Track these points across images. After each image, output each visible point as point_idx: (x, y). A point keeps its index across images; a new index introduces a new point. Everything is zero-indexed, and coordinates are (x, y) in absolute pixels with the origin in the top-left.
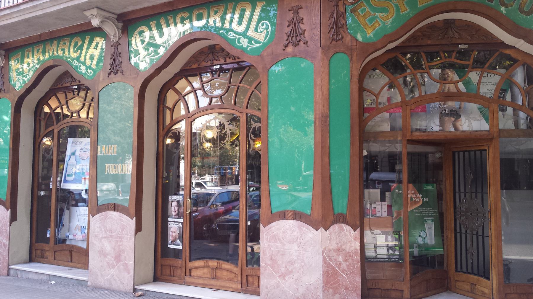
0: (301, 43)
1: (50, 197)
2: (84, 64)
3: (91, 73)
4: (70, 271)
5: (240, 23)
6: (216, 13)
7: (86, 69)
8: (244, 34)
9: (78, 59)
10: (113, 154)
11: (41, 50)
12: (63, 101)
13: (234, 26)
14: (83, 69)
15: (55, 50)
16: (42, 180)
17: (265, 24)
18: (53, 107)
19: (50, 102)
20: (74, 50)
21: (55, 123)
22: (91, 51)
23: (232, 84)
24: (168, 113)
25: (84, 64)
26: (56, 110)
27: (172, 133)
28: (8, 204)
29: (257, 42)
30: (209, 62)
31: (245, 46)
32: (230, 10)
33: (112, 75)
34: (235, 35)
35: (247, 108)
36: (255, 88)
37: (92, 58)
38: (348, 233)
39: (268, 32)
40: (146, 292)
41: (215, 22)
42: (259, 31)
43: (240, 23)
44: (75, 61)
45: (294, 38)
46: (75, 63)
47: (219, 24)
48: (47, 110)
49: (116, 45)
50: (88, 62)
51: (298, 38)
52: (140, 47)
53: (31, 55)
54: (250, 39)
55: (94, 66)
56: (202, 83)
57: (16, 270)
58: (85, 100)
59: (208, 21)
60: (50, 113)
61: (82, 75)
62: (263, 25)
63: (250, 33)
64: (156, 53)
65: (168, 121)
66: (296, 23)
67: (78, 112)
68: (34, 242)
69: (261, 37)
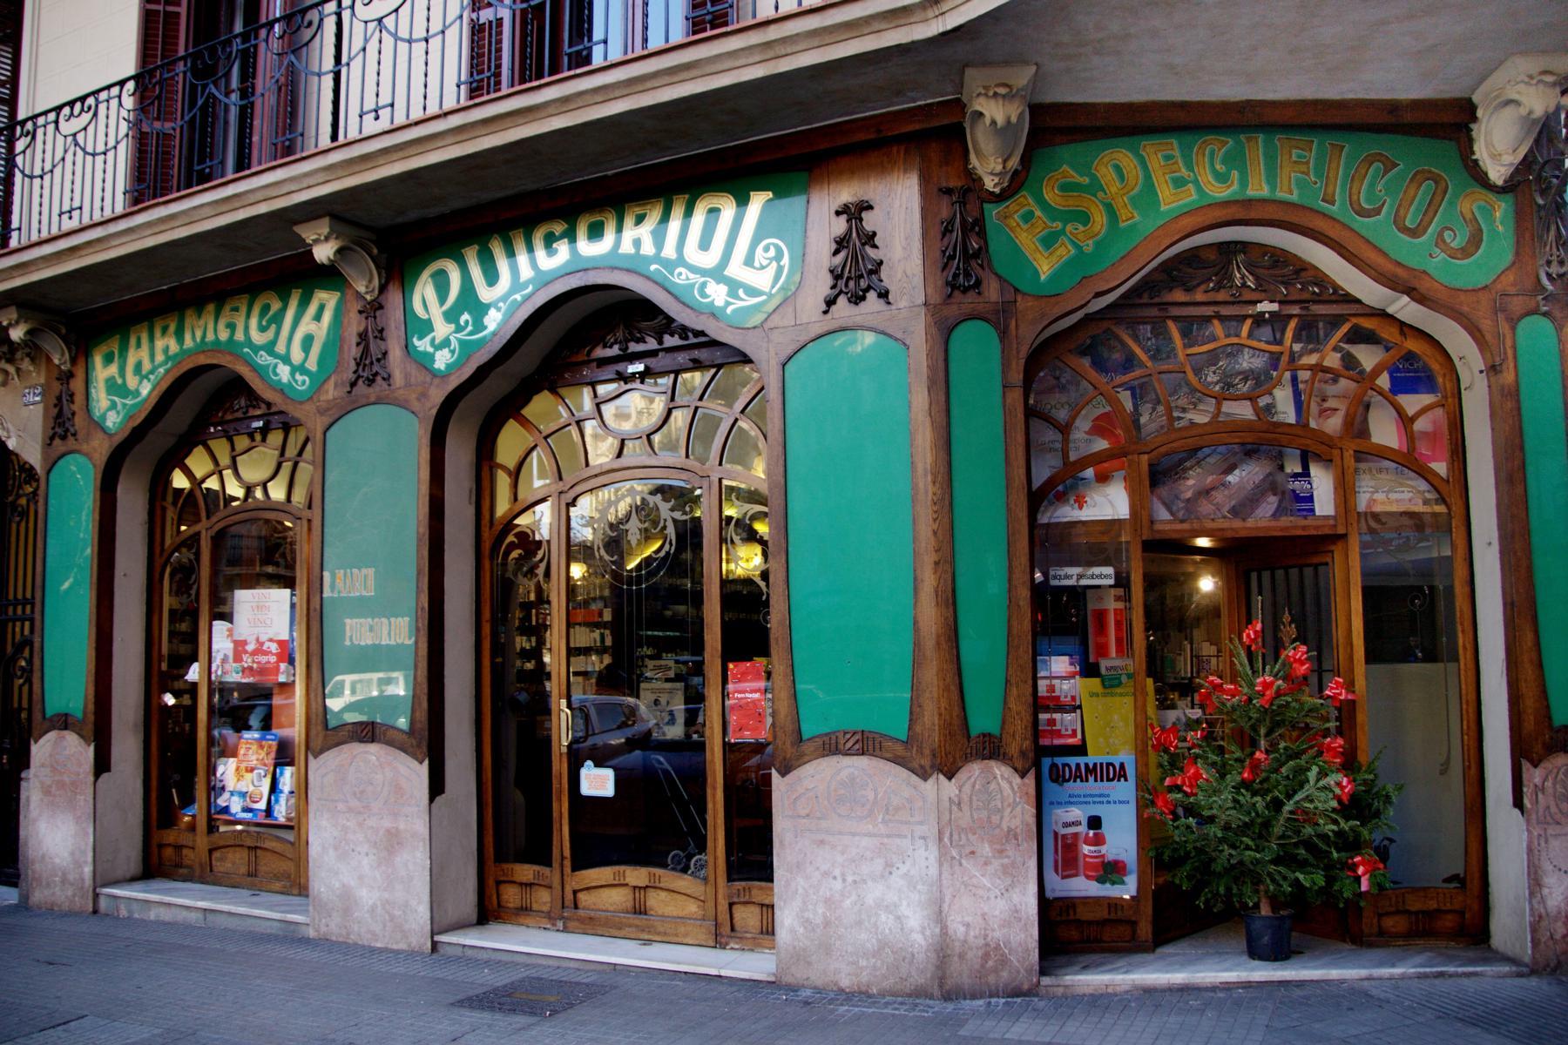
0: (872, 295)
1: (192, 711)
2: (286, 359)
3: (304, 383)
4: (255, 899)
5: (705, 245)
6: (165, 330)
7: (293, 374)
8: (718, 273)
9: (270, 348)
10: (365, 593)
11: (173, 327)
12: (224, 460)
13: (692, 253)
14: (284, 372)
15: (211, 326)
16: (169, 666)
17: (772, 248)
18: (199, 475)
19: (189, 462)
20: (260, 323)
21: (203, 514)
22: (307, 326)
23: (679, 400)
24: (503, 482)
25: (286, 359)
26: (203, 481)
27: (516, 535)
28: (89, 728)
29: (752, 291)
30: (616, 347)
31: (719, 302)
32: (678, 212)
33: (57, 441)
34: (691, 276)
35: (720, 464)
36: (742, 412)
37: (308, 341)
38: (1004, 785)
39: (780, 270)
40: (466, 949)
41: (637, 243)
42: (757, 264)
43: (705, 245)
44: (262, 353)
45: (852, 284)
46: (683, 277)
47: (648, 249)
48: (180, 481)
49: (373, 308)
50: (297, 355)
51: (863, 284)
52: (436, 313)
53: (145, 337)
54: (734, 286)
55: (312, 365)
56: (598, 401)
57: (115, 897)
58: (282, 454)
59: (618, 243)
60: (191, 491)
61: (281, 390)
62: (767, 249)
63: (735, 270)
64: (479, 326)
65: (502, 507)
66: (858, 243)
67: (264, 486)
68: (154, 823)
69: (762, 280)
